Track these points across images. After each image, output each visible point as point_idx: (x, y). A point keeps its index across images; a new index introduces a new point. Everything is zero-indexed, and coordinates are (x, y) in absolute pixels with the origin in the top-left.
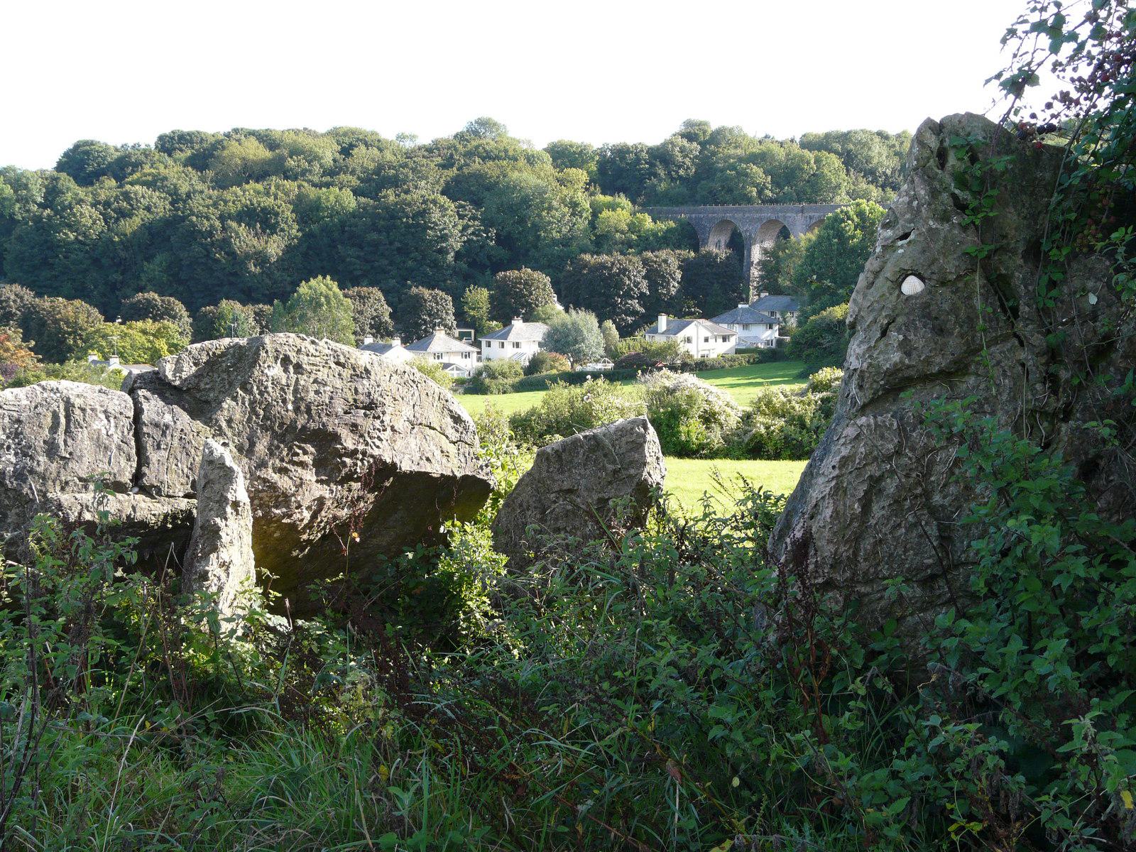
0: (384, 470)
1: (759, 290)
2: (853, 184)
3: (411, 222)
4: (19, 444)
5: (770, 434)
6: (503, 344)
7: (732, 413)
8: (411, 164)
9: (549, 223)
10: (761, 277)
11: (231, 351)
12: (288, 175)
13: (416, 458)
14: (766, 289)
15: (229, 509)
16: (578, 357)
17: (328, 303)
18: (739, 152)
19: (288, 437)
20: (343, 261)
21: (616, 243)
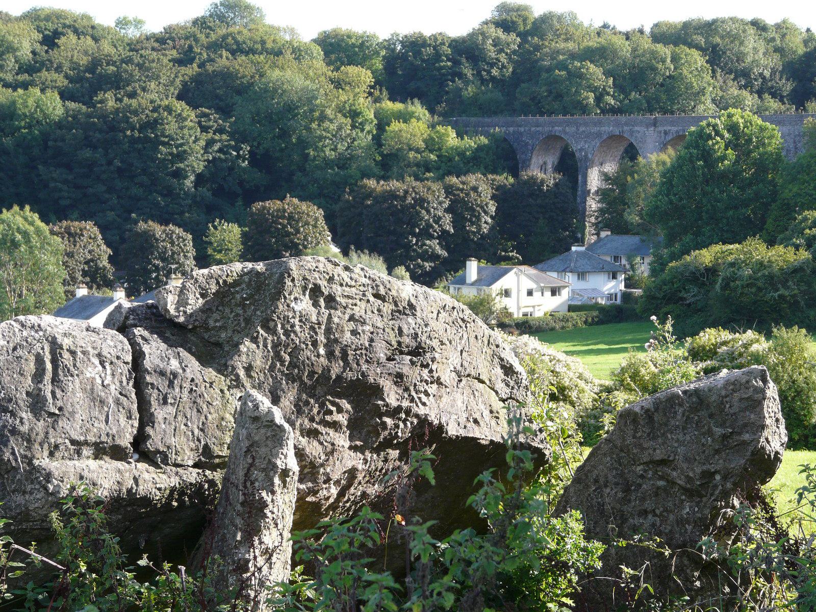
0: (428, 433)
1: (598, 227)
2: (721, 88)
3: (136, 134)
7: (587, 388)
8: (137, 59)
9: (321, 138)
10: (601, 210)
11: (246, 278)
13: (463, 420)
14: (607, 225)
15: (277, 481)
17: (27, 240)
18: (571, 45)
19: (319, 391)
20: (46, 186)
21: (409, 165)
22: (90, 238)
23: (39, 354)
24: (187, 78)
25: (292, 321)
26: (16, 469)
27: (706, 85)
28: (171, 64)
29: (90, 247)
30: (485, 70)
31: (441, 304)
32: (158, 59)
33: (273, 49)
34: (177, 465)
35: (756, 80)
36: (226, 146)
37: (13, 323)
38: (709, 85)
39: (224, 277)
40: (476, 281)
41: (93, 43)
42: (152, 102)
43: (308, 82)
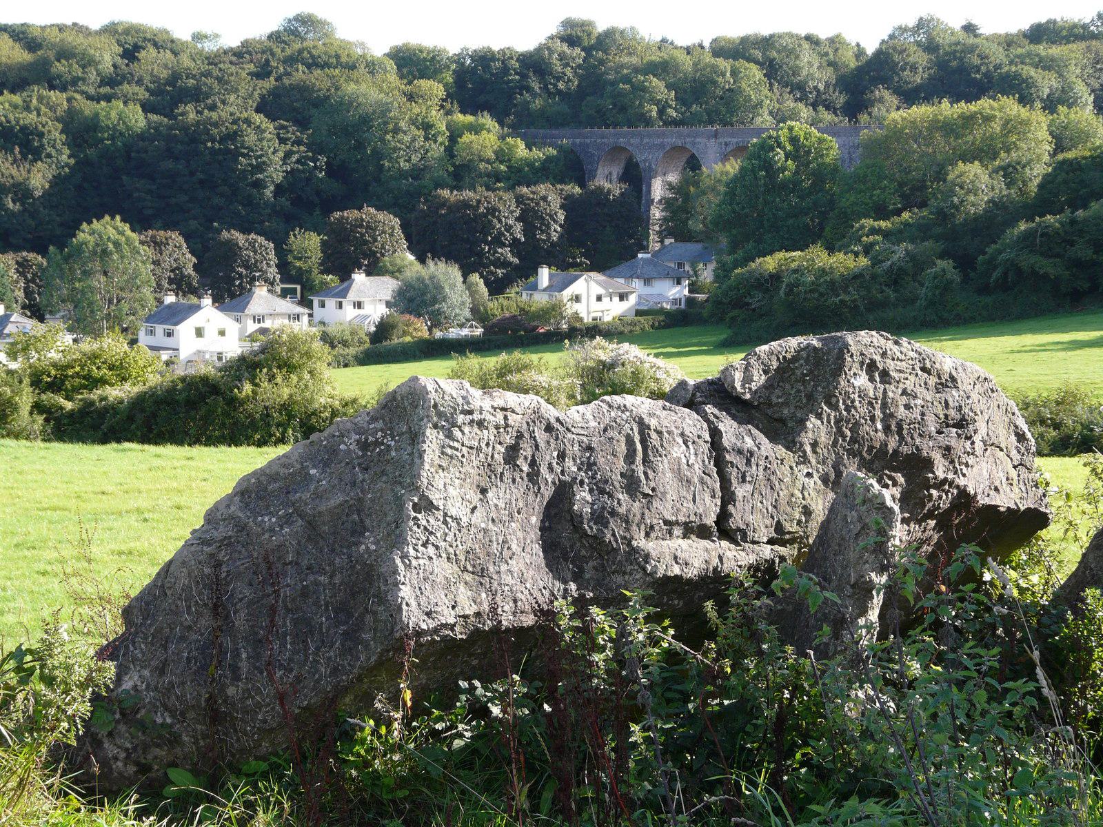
0: (964, 499)
1: (662, 236)
3: (217, 146)
4: (593, 477)
8: (216, 73)
9: (395, 149)
10: (665, 219)
11: (804, 354)
12: (53, 83)
16: (437, 321)
18: (634, 60)
22: (176, 247)
23: (629, 434)
24: (264, 92)
25: (852, 396)
26: (616, 551)
28: (249, 77)
29: (175, 256)
30: (551, 84)
31: (976, 375)
32: (237, 73)
33: (347, 63)
34: (754, 542)
35: (810, 93)
36: (303, 157)
37: (601, 404)
38: (767, 97)
39: (783, 353)
40: (547, 287)
41: (173, 57)
42: (232, 114)
43: (382, 96)
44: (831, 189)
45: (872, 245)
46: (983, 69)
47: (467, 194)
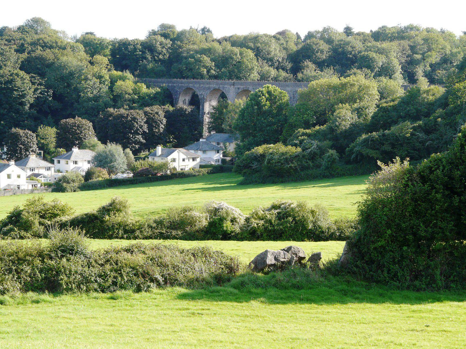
5: (258, 227)
6: (67, 161)
7: (242, 218)
9: (86, 88)
18: (195, 47)
27: (254, 66)
30: (156, 56)
33: (61, 45)
35: (276, 63)
42: (9, 71)
44: (286, 114)
45: (303, 140)
46: (353, 53)
47: (122, 111)
